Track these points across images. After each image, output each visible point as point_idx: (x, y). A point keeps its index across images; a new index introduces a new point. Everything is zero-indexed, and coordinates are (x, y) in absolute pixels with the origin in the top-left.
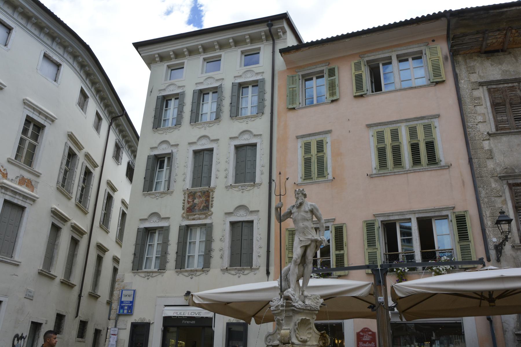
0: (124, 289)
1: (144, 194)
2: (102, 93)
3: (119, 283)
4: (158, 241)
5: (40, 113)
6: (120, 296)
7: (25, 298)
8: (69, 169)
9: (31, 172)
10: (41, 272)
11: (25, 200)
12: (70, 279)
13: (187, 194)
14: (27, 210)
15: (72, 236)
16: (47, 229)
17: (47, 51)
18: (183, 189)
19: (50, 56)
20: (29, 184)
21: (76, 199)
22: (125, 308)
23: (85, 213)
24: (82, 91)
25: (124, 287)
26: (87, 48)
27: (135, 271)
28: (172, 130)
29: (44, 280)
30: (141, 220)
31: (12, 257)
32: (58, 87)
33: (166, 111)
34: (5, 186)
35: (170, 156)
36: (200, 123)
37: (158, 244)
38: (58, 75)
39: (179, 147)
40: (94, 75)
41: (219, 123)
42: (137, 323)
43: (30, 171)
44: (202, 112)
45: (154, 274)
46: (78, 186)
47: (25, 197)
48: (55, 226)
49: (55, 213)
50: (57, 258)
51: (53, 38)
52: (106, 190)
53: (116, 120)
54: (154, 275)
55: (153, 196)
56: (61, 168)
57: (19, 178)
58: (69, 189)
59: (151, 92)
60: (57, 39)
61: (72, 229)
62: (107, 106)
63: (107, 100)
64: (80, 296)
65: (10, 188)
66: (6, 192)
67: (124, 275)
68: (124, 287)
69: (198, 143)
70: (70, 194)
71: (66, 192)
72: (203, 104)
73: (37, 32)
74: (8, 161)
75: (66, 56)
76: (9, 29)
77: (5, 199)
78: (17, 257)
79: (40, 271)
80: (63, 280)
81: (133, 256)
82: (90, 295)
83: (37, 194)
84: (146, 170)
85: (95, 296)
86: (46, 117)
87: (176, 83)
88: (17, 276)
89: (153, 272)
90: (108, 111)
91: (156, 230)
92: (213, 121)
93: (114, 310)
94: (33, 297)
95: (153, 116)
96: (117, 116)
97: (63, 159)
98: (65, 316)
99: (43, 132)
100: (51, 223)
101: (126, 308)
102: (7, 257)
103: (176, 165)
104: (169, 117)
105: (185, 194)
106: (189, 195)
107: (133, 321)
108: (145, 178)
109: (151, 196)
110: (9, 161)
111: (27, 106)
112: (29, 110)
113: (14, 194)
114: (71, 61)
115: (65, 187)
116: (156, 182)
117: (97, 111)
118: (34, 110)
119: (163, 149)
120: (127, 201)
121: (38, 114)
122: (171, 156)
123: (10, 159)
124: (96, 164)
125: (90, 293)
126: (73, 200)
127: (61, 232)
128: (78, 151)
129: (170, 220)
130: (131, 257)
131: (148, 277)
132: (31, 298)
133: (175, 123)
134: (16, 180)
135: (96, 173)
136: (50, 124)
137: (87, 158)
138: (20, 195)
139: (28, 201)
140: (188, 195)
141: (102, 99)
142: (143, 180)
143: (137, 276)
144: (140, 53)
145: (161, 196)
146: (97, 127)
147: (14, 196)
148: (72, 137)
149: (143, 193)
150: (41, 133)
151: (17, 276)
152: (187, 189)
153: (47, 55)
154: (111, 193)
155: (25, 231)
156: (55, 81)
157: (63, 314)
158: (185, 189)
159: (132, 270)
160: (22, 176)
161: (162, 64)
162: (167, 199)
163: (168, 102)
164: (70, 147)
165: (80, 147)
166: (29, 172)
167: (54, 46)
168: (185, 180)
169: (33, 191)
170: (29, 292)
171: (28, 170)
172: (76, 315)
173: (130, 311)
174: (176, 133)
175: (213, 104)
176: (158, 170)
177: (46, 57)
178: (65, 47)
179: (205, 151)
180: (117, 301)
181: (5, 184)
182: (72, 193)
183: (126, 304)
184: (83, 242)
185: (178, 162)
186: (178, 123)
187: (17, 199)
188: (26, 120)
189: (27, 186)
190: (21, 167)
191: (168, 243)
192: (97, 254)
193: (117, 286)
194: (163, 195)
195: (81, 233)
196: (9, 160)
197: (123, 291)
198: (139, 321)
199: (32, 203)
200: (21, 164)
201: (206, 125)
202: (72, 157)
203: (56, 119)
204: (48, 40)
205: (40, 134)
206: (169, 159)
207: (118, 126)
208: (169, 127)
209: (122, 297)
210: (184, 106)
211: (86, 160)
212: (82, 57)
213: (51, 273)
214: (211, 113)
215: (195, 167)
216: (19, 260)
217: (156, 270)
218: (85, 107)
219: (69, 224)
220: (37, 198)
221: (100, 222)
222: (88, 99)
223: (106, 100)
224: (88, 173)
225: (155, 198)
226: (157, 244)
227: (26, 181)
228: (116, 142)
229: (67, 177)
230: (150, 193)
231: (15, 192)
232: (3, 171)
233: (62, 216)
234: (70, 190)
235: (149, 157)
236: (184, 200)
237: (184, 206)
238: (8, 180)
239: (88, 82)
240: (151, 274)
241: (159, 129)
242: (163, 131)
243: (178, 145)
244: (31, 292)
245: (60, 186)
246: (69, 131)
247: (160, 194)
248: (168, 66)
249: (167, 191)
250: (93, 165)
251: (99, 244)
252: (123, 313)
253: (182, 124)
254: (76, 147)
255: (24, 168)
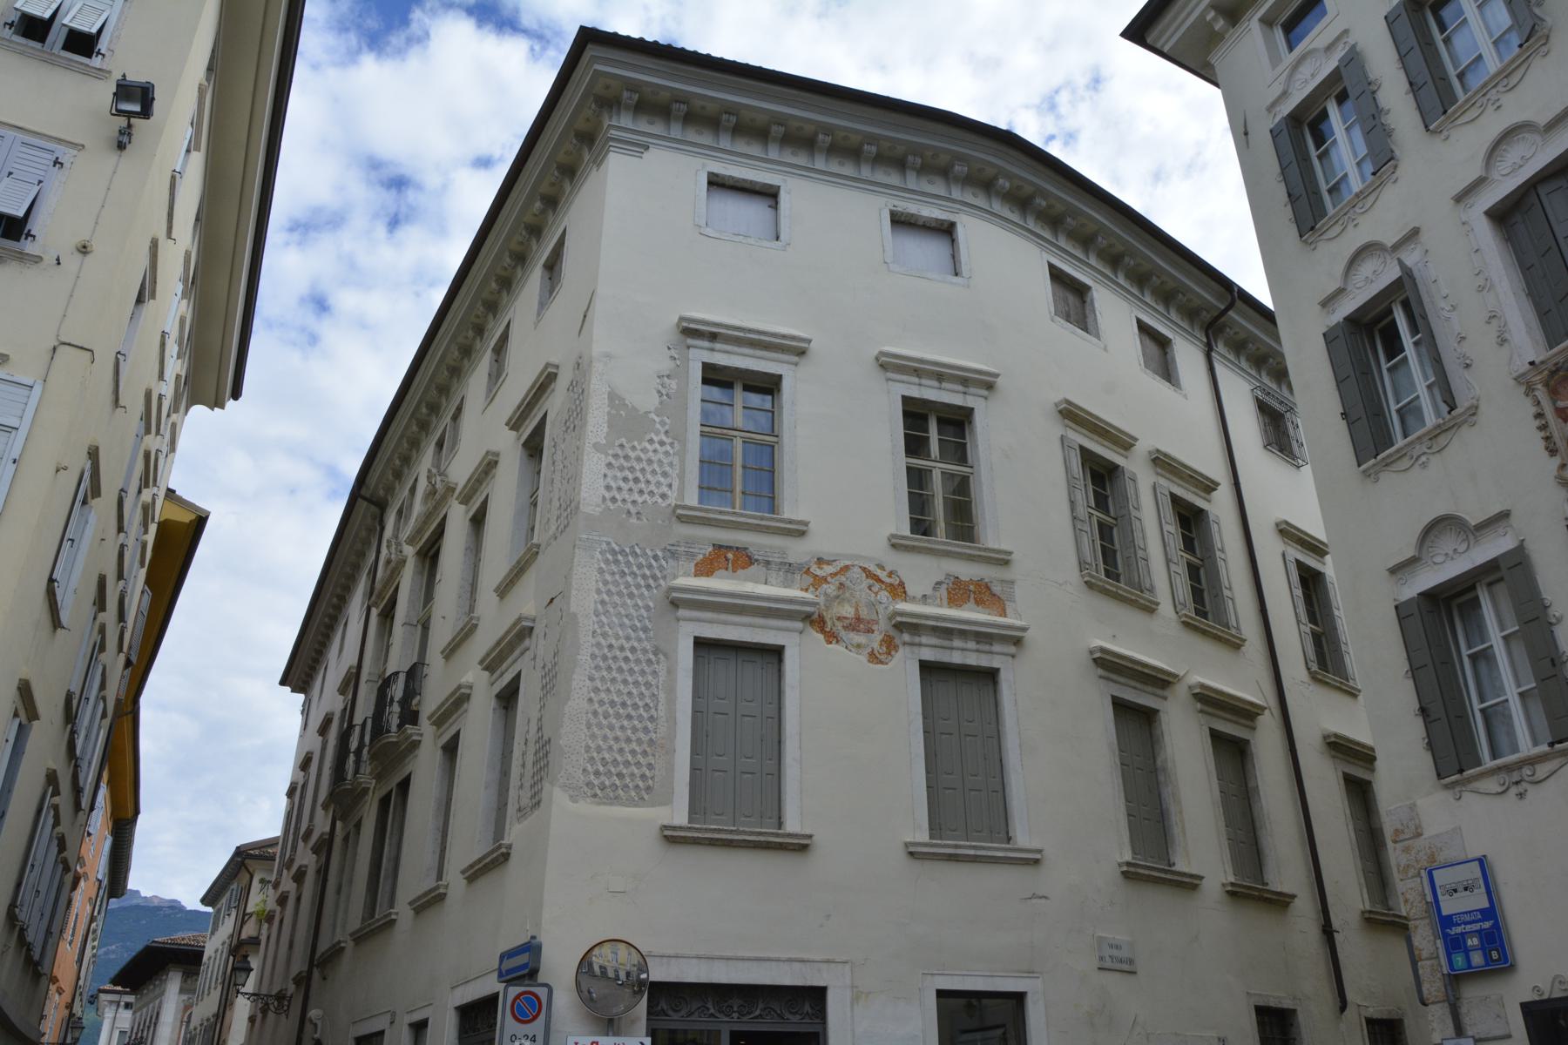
0: (1436, 865)
1: (1364, 472)
2: (1127, 259)
3: (1406, 843)
4: (1502, 629)
5: (940, 377)
6: (1430, 898)
7: (1099, 969)
8: (1116, 519)
9: (974, 556)
10: (1132, 869)
11: (986, 648)
12: (1265, 877)
13: (1539, 386)
14: (1004, 677)
15: (1211, 729)
16: (1101, 725)
17: (896, 203)
18: (1515, 375)
19: (913, 215)
20: (983, 594)
21: (1175, 607)
22: (1469, 942)
23: (1235, 644)
24: (1057, 276)
25: (1432, 858)
26: (1008, 140)
27: (1453, 778)
28: (1371, 199)
29: (1158, 900)
30: (1393, 571)
31: (1009, 839)
32: (968, 287)
33: (1324, 161)
34: (904, 619)
35: (1403, 291)
36: (1467, 101)
37: (1505, 638)
38: (956, 254)
39: (1424, 237)
40: (1076, 213)
41: (1545, 49)
42: (1549, 1000)
43: (970, 555)
44: (1456, 66)
45: (1538, 767)
46: (1168, 561)
47: (983, 637)
48: (1130, 708)
49: (1109, 665)
50: (1181, 812)
51: (899, 164)
52: (1284, 555)
53: (1221, 330)
54: (1542, 770)
55: (1405, 463)
56: (1074, 518)
57: (945, 586)
58: (1137, 580)
59: (1246, 134)
60: (910, 158)
61: (1199, 706)
62: (1167, 297)
63: (1158, 277)
64: (1328, 932)
65: (923, 622)
66: (917, 639)
67: (1413, 807)
68: (1432, 858)
69: (1495, 175)
70: (1146, 595)
71: (1216, 628)
72: (1447, 41)
73: (848, 170)
74: (894, 546)
75: (956, 193)
76: (770, 195)
77: (920, 661)
78: (1024, 837)
79: (1125, 868)
80: (1232, 884)
81: (1419, 722)
82: (1368, 920)
83: (1019, 617)
84: (1338, 386)
85: (1392, 923)
86: (965, 382)
87: (1311, 47)
88: (1046, 898)
89: (1532, 761)
90: (1128, 276)
91: (1473, 588)
92: (1518, 56)
93: (1428, 962)
94: (1131, 962)
95: (1285, 198)
96: (1216, 314)
97: (1071, 488)
98: (1294, 1011)
99: (972, 431)
100: (1110, 698)
101: (1473, 942)
102: (992, 842)
103: (1442, 304)
104: (1343, 168)
105: (1530, 390)
106: (1552, 383)
107: (1529, 997)
108: (1344, 415)
109: (1395, 467)
110: (896, 545)
111: (892, 372)
112: (903, 382)
113: (944, 639)
114: (981, 201)
115: (1122, 577)
116: (1398, 411)
117: (1139, 321)
118: (919, 376)
119: (1368, 281)
120: (1314, 526)
121: (935, 383)
122: (1409, 293)
123: (894, 536)
124: (1207, 478)
125: (1367, 915)
126: (1166, 608)
127: (1160, 724)
128: (1122, 455)
129: (1514, 519)
130: (1416, 728)
131: (1520, 788)
132: (1126, 967)
133: (1369, 168)
134: (938, 594)
135: (1220, 507)
136: (986, 398)
137: (1163, 468)
138: (963, 634)
139: (997, 648)
140: (1546, 385)
141: (1141, 279)
142: (1342, 426)
143: (1467, 796)
144: (1158, 46)
145: (1435, 449)
146: (1167, 372)
147: (946, 643)
148: (1077, 415)
149: (1364, 467)
150: (970, 433)
151: (1046, 898)
152: (1532, 363)
153: (902, 213)
154: (1311, 561)
155: (1020, 746)
156: (956, 275)
157: (1285, 1006)
158: (1522, 371)
159: (1440, 776)
160: (952, 578)
161: (1240, 28)
162: (1467, 447)
163: (1321, 131)
164: (1082, 448)
165: (1125, 443)
166: (971, 558)
167: (912, 181)
168: (1507, 336)
169: (1003, 613)
170: (1111, 946)
171: (965, 554)
172: (1339, 1004)
173: (1495, 955)
174: (1390, 195)
175: (1487, 10)
176: (1385, 366)
177: (901, 222)
178: (945, 173)
179: (1543, 191)
180: (1427, 921)
181: (902, 614)
182: (1151, 590)
183: (1469, 928)
184: (1266, 743)
185: (1445, 292)
186: (1382, 159)
187: (959, 652)
188: (906, 414)
189: (978, 602)
190: (938, 550)
191: (1546, 615)
192: (1341, 774)
193: (1395, 856)
194: (1442, 440)
195: (1247, 713)
196: (894, 541)
197: (1435, 873)
198: (1557, 994)
199: (1012, 649)
200: (939, 543)
201: (1494, 91)
202: (1110, 480)
203: (997, 376)
204: (889, 175)
205: (968, 440)
206: (1406, 305)
207: (1238, 347)
208: (1357, 195)
209: (1440, 897)
210: (1374, 92)
211: (1162, 476)
212: (1009, 176)
213: (1177, 868)
214: (1495, 43)
215: (1526, 269)
216: (1035, 845)
217: (1544, 748)
218: (1090, 320)
219: (1180, 692)
220: (1024, 629)
221: (1306, 663)
222: (1089, 294)
223: (1154, 278)
224: (1190, 520)
225: (1417, 465)
226: (1501, 642)
227: (972, 587)
228: (1257, 399)
229: (1117, 546)
230: (1388, 456)
231: (945, 632)
232: (888, 580)
233: (1140, 669)
234: (1139, 582)
235: (1330, 338)
236: (1539, 416)
237: (1547, 439)
238: (913, 600)
239: (1062, 242)
240: (1527, 771)
241: (1323, 225)
242: (1340, 222)
243: (1415, 232)
244: (1117, 947)
245: (1103, 577)
246: (1056, 400)
247: (1429, 443)
248: (1262, 20)
249: (1448, 417)
250: (1196, 487)
251: (1333, 739)
252: (1470, 967)
253: (1397, 152)
254: (1106, 443)
255: (950, 552)
